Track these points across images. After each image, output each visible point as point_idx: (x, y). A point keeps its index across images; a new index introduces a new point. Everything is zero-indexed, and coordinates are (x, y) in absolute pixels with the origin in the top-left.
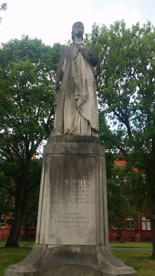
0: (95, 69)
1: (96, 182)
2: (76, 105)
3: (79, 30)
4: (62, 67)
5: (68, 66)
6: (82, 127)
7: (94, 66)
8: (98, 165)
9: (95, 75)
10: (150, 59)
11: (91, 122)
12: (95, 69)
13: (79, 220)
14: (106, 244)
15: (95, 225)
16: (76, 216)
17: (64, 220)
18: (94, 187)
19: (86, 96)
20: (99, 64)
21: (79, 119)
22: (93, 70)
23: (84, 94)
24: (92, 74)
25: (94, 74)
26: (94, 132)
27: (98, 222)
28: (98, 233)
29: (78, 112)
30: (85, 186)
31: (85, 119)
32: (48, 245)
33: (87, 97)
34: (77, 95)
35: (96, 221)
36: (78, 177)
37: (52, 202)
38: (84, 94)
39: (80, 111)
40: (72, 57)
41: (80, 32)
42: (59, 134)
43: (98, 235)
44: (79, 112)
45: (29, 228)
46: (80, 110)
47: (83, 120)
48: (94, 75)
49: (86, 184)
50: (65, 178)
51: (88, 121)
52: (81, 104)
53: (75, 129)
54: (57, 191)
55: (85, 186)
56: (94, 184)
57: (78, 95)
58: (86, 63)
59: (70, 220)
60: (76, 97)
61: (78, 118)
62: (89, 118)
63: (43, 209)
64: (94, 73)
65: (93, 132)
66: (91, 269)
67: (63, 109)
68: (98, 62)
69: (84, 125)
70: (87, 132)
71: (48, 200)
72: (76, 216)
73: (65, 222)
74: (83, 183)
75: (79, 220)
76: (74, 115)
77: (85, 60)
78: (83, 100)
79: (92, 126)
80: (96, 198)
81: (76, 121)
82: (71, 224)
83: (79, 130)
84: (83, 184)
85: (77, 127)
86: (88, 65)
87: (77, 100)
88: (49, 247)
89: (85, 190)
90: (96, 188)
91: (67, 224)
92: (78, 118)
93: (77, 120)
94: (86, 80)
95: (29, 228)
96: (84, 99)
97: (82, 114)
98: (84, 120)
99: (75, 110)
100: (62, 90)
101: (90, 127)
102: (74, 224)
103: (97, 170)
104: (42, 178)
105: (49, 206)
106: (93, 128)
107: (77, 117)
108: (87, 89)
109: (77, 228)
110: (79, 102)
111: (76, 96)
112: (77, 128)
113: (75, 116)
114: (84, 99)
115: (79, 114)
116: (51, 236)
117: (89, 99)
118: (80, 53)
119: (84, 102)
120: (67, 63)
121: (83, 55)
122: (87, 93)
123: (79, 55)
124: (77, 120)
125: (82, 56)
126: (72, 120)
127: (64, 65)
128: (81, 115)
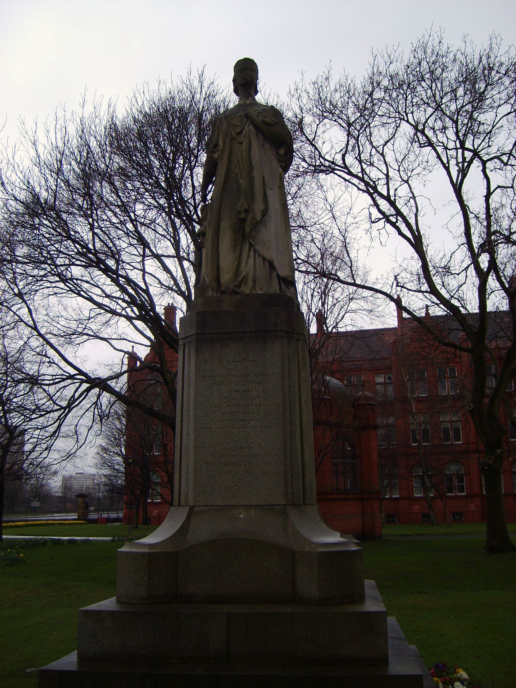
0: (282, 151)
5: (227, 152)
9: (283, 164)
10: (130, 463)
11: (276, 264)
21: (251, 260)
22: (277, 153)
25: (282, 162)
26: (285, 285)
31: (264, 259)
32: (194, 506)
47: (259, 261)
48: (280, 165)
58: (261, 142)
60: (242, 216)
61: (248, 257)
63: (184, 442)
79: (278, 272)
81: (243, 265)
83: (250, 283)
86: (267, 146)
92: (248, 257)
97: (258, 248)
98: (261, 259)
104: (314, 453)
106: (281, 275)
107: (245, 255)
111: (242, 214)
112: (247, 279)
113: (241, 253)
118: (248, 124)
120: (224, 143)
123: (246, 127)
125: (252, 127)
127: (218, 148)
128: (255, 251)
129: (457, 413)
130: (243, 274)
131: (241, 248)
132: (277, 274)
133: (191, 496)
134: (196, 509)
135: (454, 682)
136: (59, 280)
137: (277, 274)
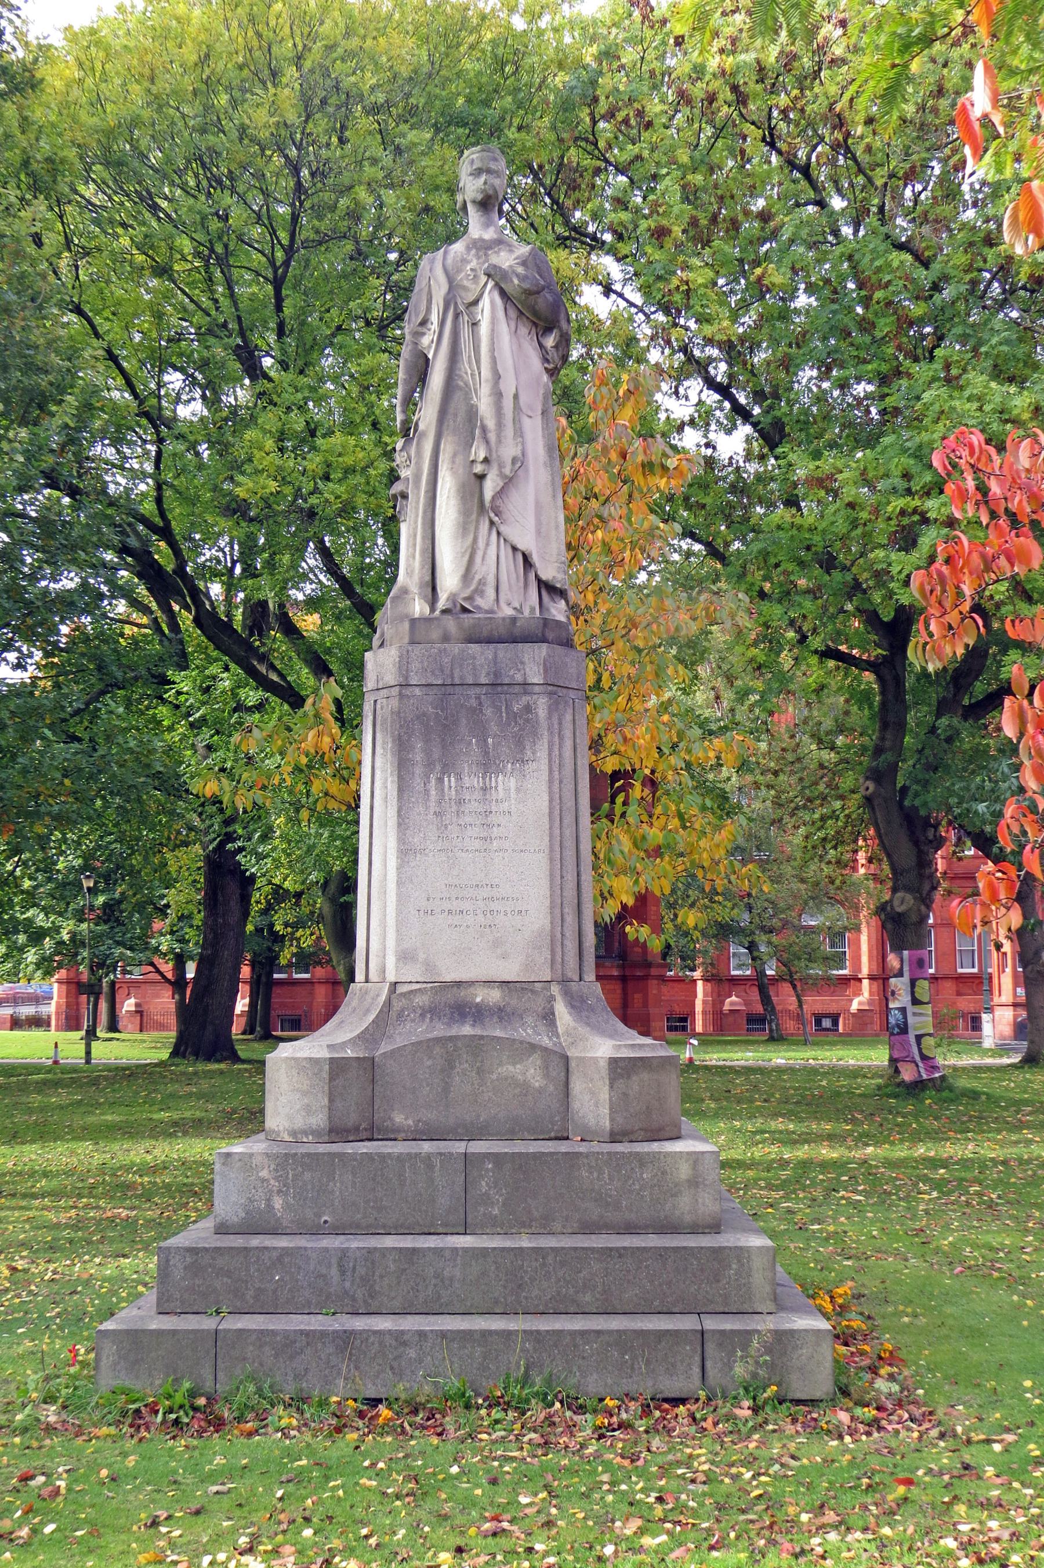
0: (550, 341)
1: (551, 781)
2: (477, 495)
3: (485, 183)
4: (424, 334)
6: (504, 577)
7: (548, 330)
8: (560, 724)
11: (535, 559)
12: (550, 341)
13: (495, 906)
14: (586, 978)
15: (547, 922)
16: (485, 893)
17: (446, 906)
18: (546, 797)
19: (514, 460)
20: (564, 325)
22: (541, 345)
23: (509, 451)
24: (536, 363)
27: (558, 911)
28: (559, 944)
29: (487, 522)
30: (513, 795)
31: (515, 549)
33: (520, 462)
34: (481, 459)
35: (552, 907)
36: (488, 765)
37: (405, 852)
38: (509, 451)
39: (496, 519)
40: (459, 301)
41: (491, 192)
42: (419, 608)
43: (559, 950)
44: (492, 523)
45: (276, 976)
46: (492, 515)
47: (505, 553)
49: (518, 790)
50: (446, 769)
51: (524, 555)
52: (500, 493)
53: (476, 591)
54: (419, 814)
55: (513, 795)
56: (544, 787)
57: (486, 461)
58: (513, 324)
59: (466, 905)
60: (478, 469)
62: (526, 542)
64: (546, 360)
65: (544, 593)
66: (533, 1047)
67: (429, 514)
68: (562, 316)
69: (510, 569)
70: (522, 598)
71: (392, 843)
72: (485, 893)
73: (450, 912)
74: (505, 784)
75: (495, 906)
76: (471, 536)
77: (512, 313)
78: (506, 477)
80: (551, 836)
81: (478, 559)
82: (470, 919)
84: (507, 790)
85: (482, 582)
86: (523, 330)
87: (481, 477)
88: (402, 989)
89: (513, 809)
90: (551, 801)
91: (456, 919)
92: (488, 544)
93: (485, 553)
94: (516, 397)
95: (276, 976)
96: (507, 471)
97: (502, 529)
99: (474, 516)
100: (424, 434)
101: (532, 576)
102: (481, 918)
103: (556, 739)
105: (392, 862)
107: (481, 543)
108: (519, 433)
109: (488, 930)
110: (490, 487)
112: (484, 584)
113: (475, 540)
114: (507, 471)
115: (490, 529)
116: (405, 957)
117: (527, 471)
119: (509, 483)
120: (442, 324)
121: (503, 293)
122: (520, 447)
124: (485, 553)
126: (463, 554)
127: (429, 326)
128: (499, 533)
129: (632, 1368)
130: (477, 577)
131: (477, 528)
132: (536, 576)
133: (391, 962)
134: (402, 989)
135: (887, 623)
136: (170, 975)
137: (536, 576)
